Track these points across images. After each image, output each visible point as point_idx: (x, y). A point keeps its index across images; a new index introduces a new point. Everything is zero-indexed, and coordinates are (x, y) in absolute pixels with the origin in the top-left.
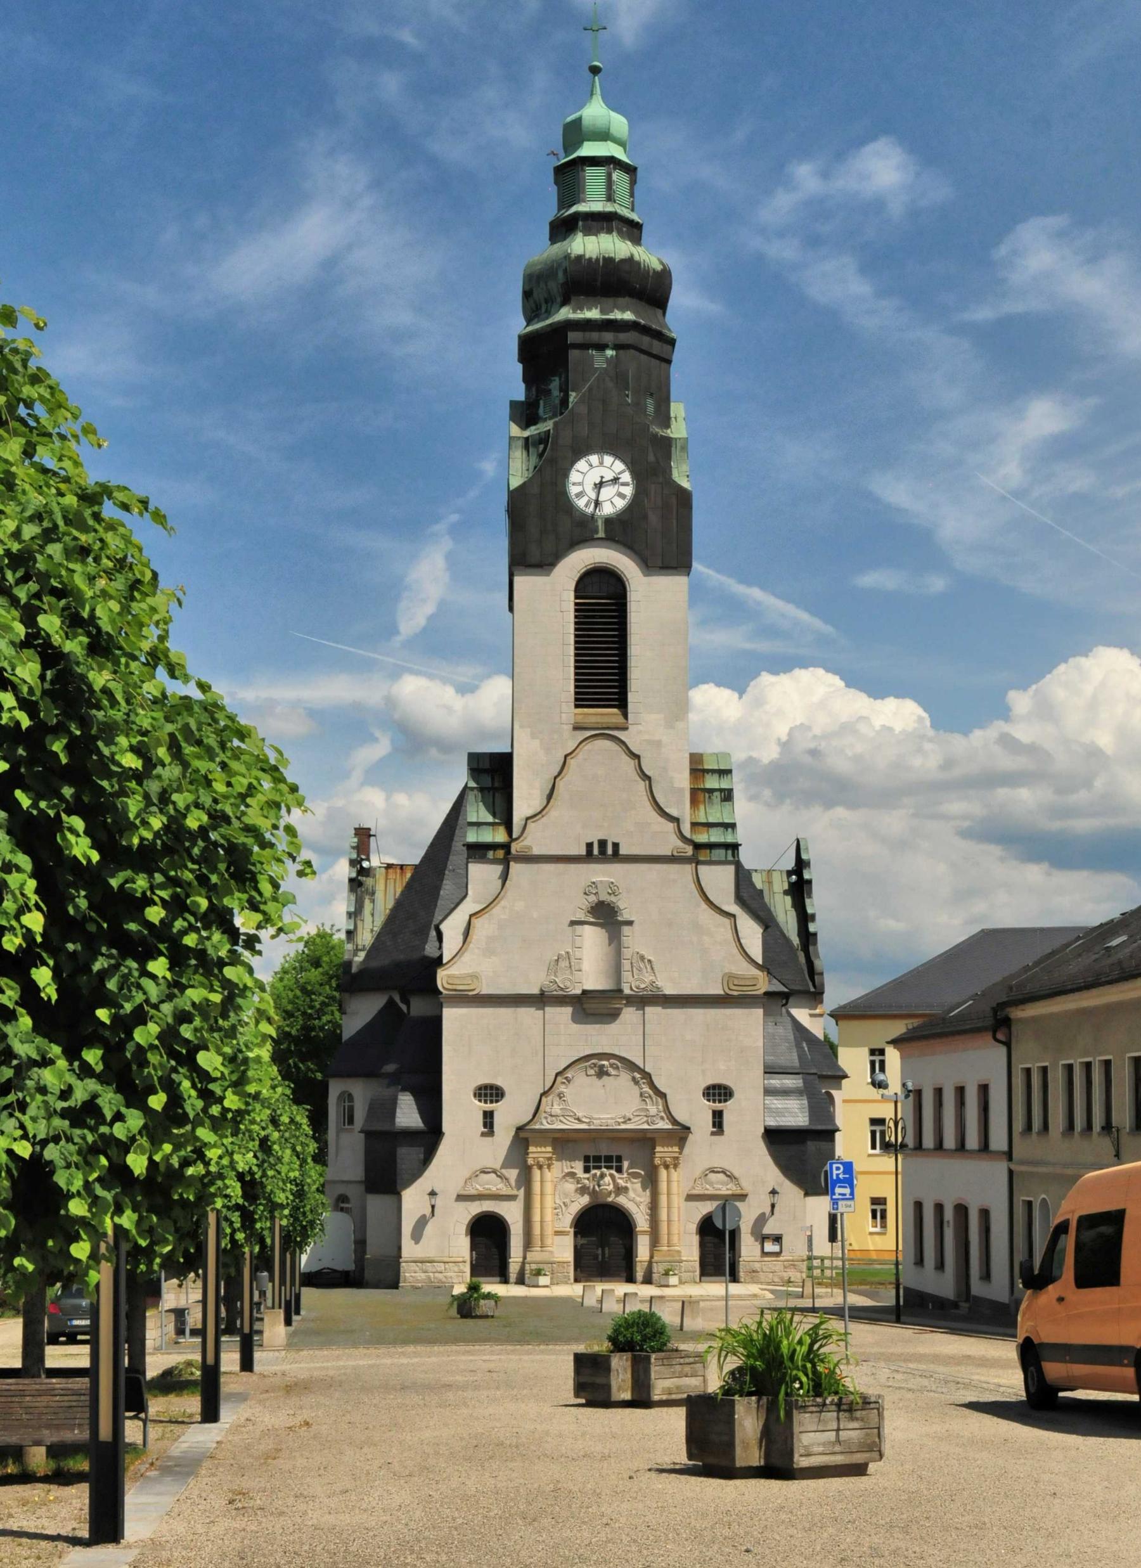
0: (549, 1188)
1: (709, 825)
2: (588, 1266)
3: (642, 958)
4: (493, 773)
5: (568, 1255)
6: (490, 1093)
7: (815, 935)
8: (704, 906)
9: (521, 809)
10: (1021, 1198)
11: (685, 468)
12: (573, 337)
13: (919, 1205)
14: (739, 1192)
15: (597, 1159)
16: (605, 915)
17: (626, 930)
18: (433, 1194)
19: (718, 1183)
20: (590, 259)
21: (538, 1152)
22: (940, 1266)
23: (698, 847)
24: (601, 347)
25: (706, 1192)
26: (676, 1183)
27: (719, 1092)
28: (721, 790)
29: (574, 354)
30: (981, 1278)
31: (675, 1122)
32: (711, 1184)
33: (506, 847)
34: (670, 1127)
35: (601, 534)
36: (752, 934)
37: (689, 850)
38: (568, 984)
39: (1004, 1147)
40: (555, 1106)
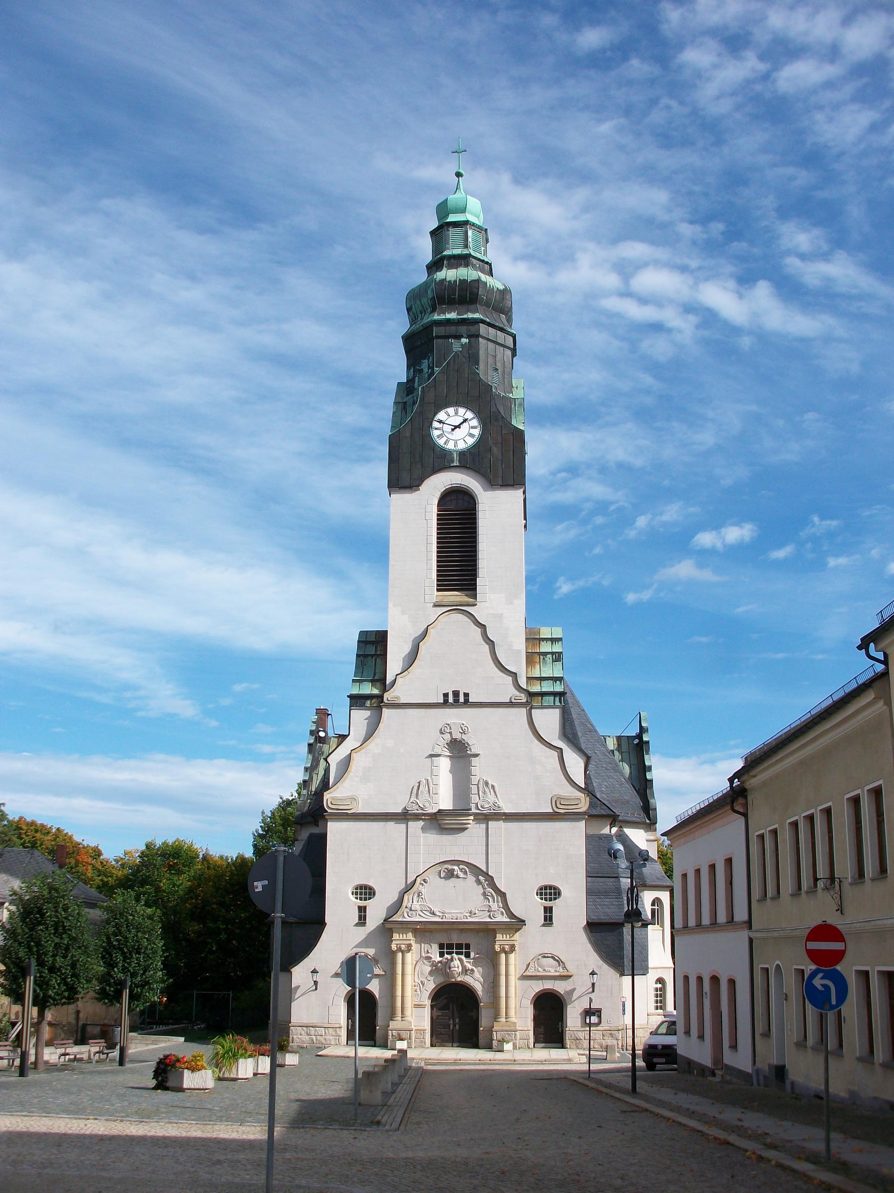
0: (409, 969)
1: (542, 679)
2: (441, 1034)
3: (487, 783)
6: (365, 892)
7: (651, 781)
9: (394, 665)
10: (758, 966)
11: (521, 418)
12: (436, 331)
13: (686, 978)
14: (566, 973)
15: (450, 946)
16: (459, 750)
18: (314, 972)
20: (450, 281)
22: (701, 1037)
23: (532, 695)
24: (458, 337)
25: (539, 974)
26: (513, 966)
27: (550, 892)
28: (552, 653)
30: (730, 1047)
31: (511, 915)
33: (380, 697)
35: (456, 463)
36: (575, 764)
38: (427, 805)
39: (745, 918)
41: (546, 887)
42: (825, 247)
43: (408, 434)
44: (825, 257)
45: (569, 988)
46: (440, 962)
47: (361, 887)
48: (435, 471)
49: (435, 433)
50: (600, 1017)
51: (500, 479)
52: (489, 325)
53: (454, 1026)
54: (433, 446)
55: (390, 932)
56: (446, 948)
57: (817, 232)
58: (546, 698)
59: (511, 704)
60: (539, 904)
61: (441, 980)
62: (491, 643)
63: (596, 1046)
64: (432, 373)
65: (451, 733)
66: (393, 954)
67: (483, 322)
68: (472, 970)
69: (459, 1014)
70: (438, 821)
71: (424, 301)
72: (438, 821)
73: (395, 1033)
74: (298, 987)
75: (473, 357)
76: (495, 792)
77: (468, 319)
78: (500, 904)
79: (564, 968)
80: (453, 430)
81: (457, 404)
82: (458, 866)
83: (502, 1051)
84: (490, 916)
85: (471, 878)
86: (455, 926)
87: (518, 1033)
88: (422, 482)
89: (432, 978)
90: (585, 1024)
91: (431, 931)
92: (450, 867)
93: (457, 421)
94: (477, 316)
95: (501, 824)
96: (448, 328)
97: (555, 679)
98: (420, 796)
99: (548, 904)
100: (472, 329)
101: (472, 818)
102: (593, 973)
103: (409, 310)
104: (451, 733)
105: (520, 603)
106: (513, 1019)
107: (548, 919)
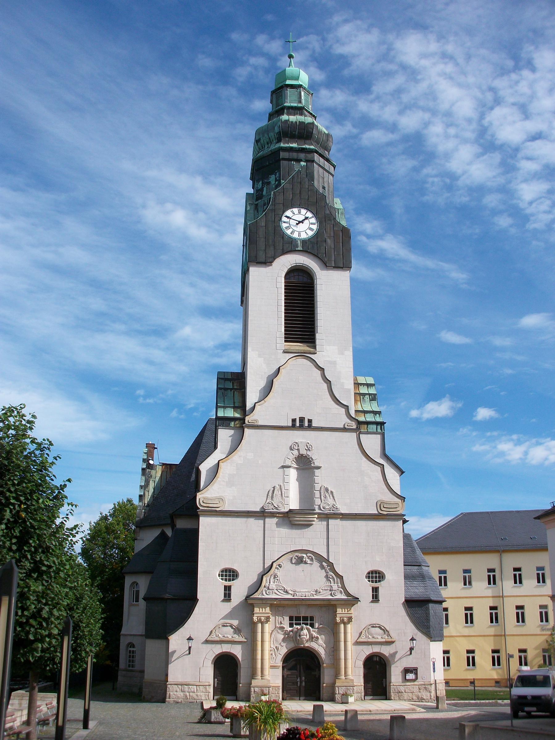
1: (365, 412)
2: (291, 690)
3: (327, 490)
4: (232, 385)
5: (279, 682)
6: (230, 574)
8: (364, 459)
9: (252, 397)
12: (282, 155)
14: (390, 640)
15: (298, 618)
16: (305, 464)
17: (317, 472)
19: (376, 634)
20: (292, 122)
21: (259, 612)
23: (359, 423)
24: (298, 161)
25: (369, 640)
26: (350, 633)
27: (376, 576)
28: (369, 394)
29: (283, 163)
31: (348, 594)
32: (371, 634)
33: (242, 420)
34: (346, 598)
37: (354, 425)
38: (280, 505)
40: (272, 583)
41: (372, 572)
42: (380, 231)
43: (263, 224)
44: (380, 237)
45: (392, 652)
46: (292, 631)
47: (226, 570)
48: (284, 253)
49: (284, 225)
50: (416, 674)
51: (333, 262)
52: (321, 155)
53: (301, 682)
54: (283, 235)
55: (252, 606)
56: (294, 620)
57: (376, 223)
58: (370, 426)
59: (344, 429)
60: (221, 583)
61: (292, 645)
62: (328, 382)
63: (414, 698)
64: (279, 184)
65: (298, 450)
66: (254, 624)
67: (317, 152)
68: (317, 638)
69: (305, 672)
70: (289, 519)
71: (271, 134)
72: (289, 519)
73: (256, 689)
74: (174, 652)
75: (311, 177)
76: (333, 497)
77: (306, 149)
78: (340, 585)
79: (389, 635)
80: (297, 224)
81: (300, 206)
82: (306, 554)
83: (347, 703)
84: (331, 595)
85: (316, 564)
86: (304, 603)
87: (355, 688)
88: (274, 259)
89: (284, 644)
90: (405, 680)
91: (284, 606)
92: (300, 555)
93: (301, 218)
94: (312, 147)
95: (338, 521)
96: (291, 153)
97: (375, 413)
98: (274, 499)
99: (228, 583)
100: (309, 156)
101: (316, 516)
102: (413, 639)
103: (257, 141)
104: (298, 450)
105: (349, 354)
106: (350, 677)
107: (375, 598)
